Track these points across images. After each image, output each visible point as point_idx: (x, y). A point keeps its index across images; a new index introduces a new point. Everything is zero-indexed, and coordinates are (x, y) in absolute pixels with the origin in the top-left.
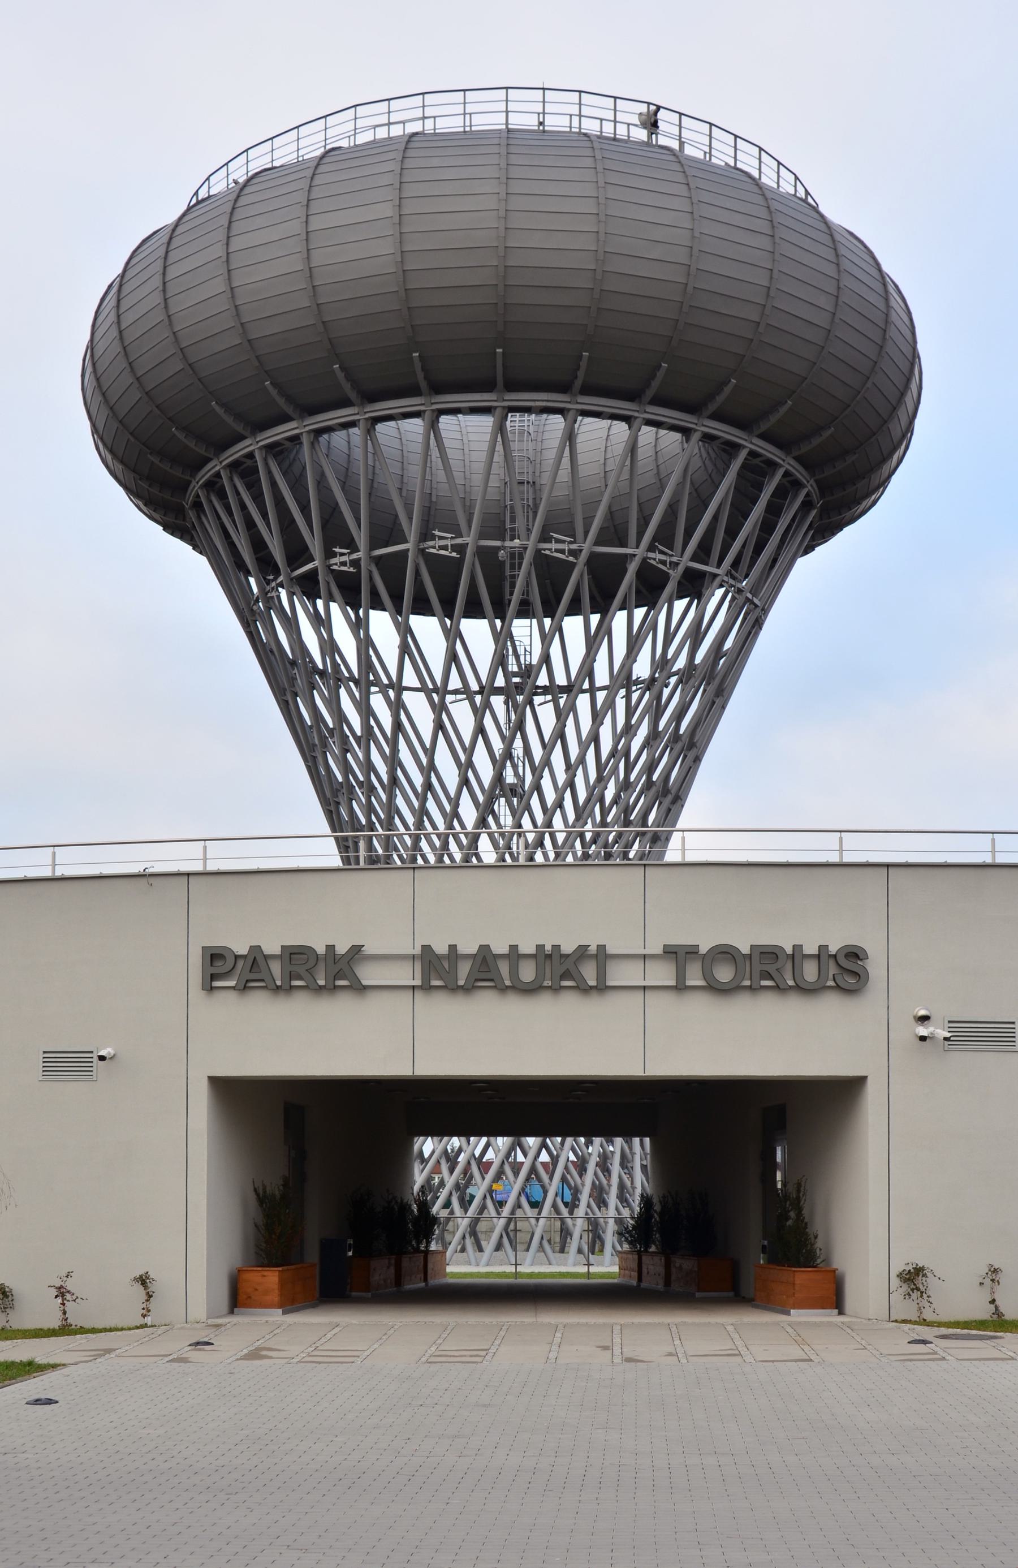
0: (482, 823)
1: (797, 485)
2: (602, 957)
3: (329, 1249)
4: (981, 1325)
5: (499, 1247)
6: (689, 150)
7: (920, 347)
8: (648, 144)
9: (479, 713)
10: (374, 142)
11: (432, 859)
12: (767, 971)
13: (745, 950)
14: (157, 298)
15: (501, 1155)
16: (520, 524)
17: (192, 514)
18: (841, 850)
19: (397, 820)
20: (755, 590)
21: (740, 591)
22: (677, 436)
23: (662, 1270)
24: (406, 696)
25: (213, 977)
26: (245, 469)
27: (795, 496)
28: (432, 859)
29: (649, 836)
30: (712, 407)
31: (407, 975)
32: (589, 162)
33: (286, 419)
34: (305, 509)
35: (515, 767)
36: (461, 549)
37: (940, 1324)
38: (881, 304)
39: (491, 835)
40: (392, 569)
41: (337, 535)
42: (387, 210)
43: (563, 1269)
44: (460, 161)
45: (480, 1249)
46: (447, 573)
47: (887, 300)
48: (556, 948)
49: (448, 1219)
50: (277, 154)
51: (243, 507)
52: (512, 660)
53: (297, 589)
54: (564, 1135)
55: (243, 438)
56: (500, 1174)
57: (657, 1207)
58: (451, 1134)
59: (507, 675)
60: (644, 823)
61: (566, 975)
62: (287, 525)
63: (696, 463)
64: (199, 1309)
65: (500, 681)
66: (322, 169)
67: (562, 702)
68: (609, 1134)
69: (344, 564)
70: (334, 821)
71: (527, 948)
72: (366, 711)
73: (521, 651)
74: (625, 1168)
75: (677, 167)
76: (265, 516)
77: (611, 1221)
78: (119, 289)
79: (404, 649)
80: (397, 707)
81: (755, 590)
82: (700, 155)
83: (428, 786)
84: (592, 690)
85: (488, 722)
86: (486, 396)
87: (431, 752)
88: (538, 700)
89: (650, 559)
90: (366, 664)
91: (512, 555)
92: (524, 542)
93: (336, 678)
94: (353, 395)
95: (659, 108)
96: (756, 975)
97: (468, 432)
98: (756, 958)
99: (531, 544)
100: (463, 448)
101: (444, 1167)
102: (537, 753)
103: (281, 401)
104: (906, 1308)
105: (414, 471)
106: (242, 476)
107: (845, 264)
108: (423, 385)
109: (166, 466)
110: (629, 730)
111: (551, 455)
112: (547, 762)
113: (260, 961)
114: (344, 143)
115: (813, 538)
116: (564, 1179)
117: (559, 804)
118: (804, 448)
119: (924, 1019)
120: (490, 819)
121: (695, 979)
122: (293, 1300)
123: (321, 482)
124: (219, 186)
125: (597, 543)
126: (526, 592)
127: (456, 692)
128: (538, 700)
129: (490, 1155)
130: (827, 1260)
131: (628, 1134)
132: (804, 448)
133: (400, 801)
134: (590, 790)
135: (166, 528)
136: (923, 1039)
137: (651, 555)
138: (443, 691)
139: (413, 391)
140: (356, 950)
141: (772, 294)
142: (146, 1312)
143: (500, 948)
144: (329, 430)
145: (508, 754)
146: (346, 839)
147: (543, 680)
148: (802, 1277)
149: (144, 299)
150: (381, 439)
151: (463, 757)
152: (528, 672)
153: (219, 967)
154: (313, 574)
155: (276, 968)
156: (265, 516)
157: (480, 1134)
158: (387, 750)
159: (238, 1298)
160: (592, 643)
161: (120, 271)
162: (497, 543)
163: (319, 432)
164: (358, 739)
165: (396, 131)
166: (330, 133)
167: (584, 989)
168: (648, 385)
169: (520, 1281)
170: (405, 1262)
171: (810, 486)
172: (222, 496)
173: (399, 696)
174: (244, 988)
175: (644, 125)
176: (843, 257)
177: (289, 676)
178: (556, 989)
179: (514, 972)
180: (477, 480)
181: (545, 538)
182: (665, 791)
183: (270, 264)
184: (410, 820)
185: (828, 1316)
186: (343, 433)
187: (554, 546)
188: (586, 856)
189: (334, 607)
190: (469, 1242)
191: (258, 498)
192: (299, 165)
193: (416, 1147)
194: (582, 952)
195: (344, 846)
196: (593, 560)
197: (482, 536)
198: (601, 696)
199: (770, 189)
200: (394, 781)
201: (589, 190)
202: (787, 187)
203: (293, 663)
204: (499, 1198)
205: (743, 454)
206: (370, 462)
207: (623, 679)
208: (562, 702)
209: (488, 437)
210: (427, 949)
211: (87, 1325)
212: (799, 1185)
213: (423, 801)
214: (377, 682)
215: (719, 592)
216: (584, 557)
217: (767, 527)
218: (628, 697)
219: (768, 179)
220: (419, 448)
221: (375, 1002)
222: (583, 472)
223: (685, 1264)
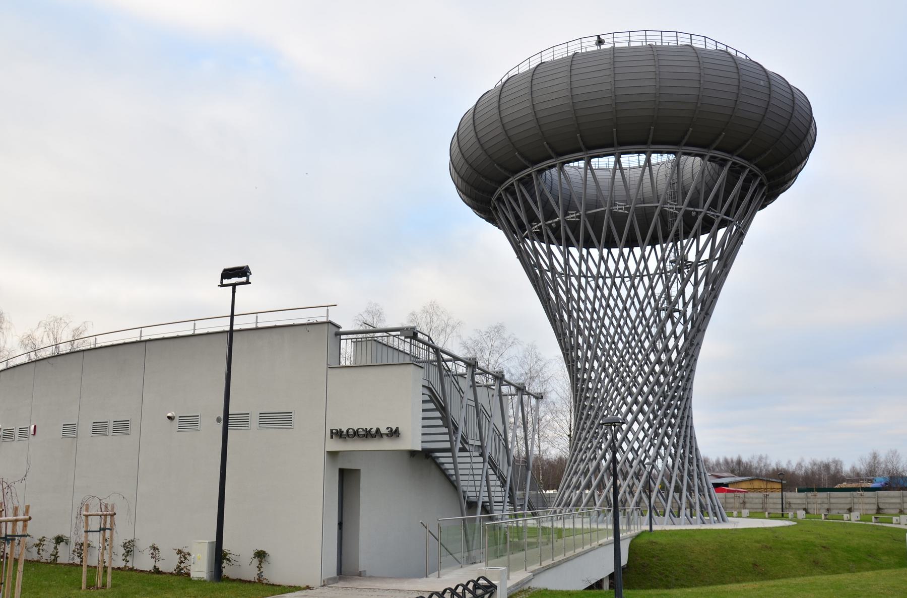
26: (510, 190)
30: (684, 142)
44: (597, 63)
62: (528, 210)
94: (553, 154)
97: (603, 163)
108: (583, 147)
115: (766, 200)
123: (542, 193)
171: (762, 177)
191: (516, 200)
205: (729, 164)
216: (682, 212)
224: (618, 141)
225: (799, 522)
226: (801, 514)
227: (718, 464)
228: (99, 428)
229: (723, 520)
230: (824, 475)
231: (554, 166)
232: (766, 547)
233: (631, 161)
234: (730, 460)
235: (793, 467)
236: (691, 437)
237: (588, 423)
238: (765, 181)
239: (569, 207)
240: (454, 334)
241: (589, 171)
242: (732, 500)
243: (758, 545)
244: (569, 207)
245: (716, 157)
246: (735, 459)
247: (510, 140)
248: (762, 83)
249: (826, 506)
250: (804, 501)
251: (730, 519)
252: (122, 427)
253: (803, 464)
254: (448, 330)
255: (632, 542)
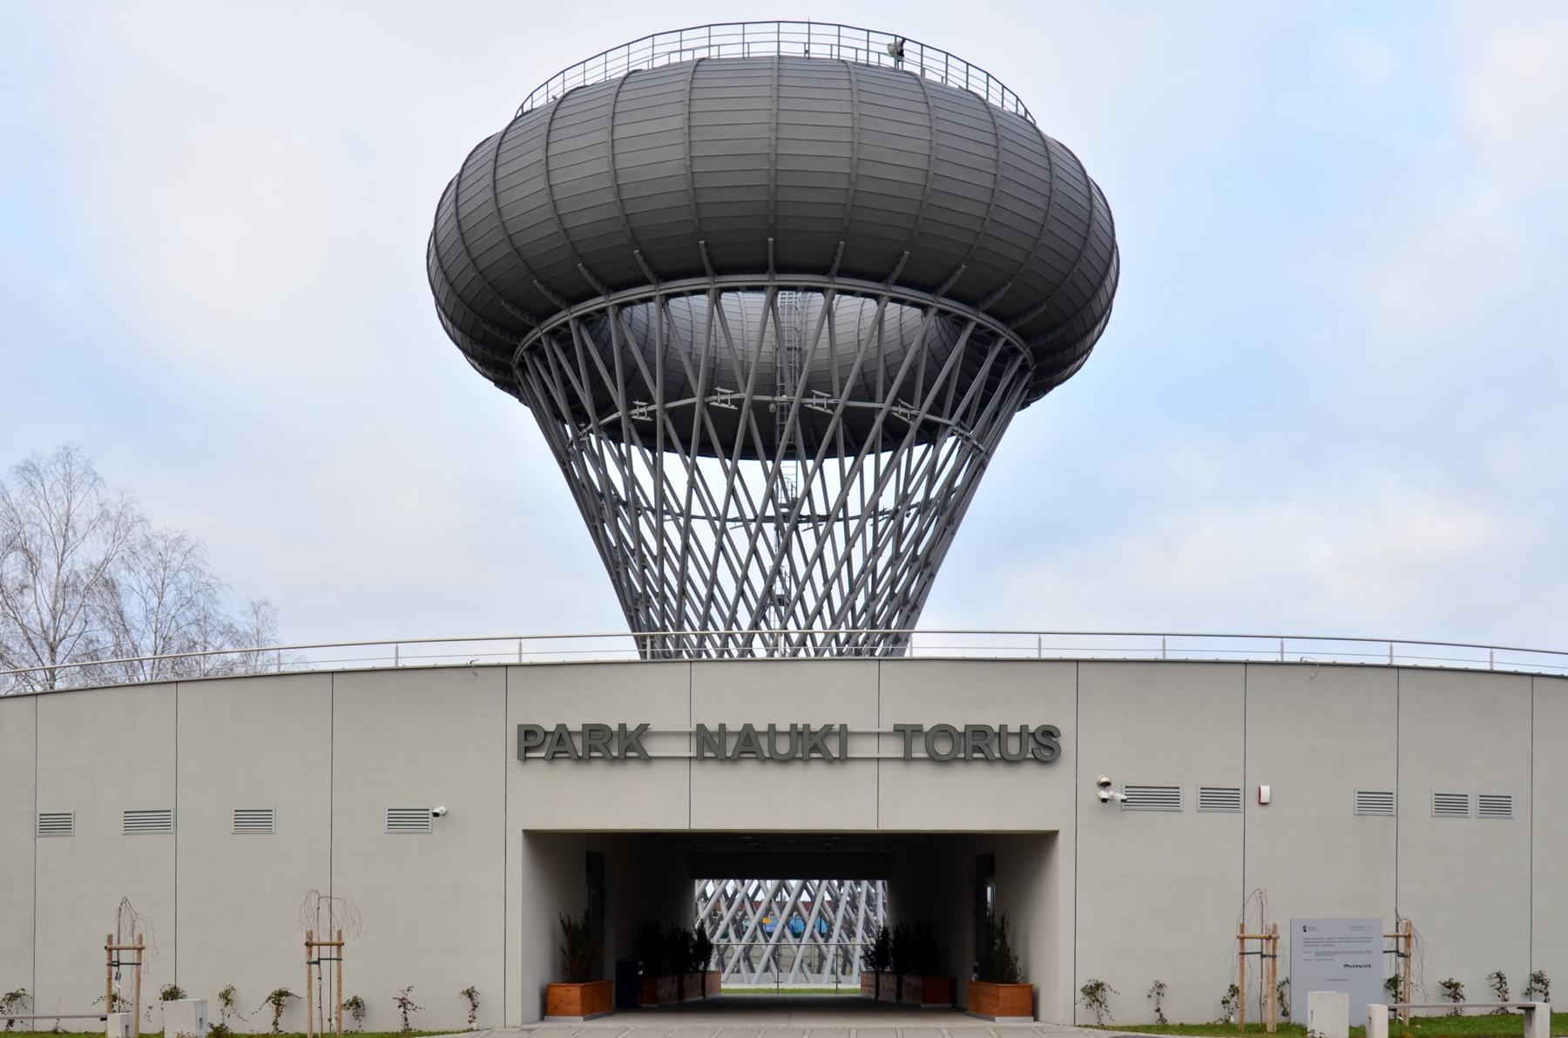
0: (755, 625)
1: (1015, 352)
2: (844, 734)
3: (625, 969)
4: (1148, 1028)
5: (767, 969)
6: (929, 76)
7: (1118, 239)
8: (895, 70)
9: (753, 539)
10: (669, 65)
11: (714, 655)
12: (977, 746)
13: (961, 729)
14: (489, 194)
15: (770, 894)
16: (788, 385)
17: (518, 373)
18: (1040, 649)
19: (686, 625)
20: (980, 439)
21: (967, 439)
22: (918, 311)
23: (894, 986)
24: (694, 523)
25: (527, 749)
26: (561, 336)
27: (1014, 361)
28: (714, 655)
29: (891, 638)
30: (946, 288)
31: (685, 748)
32: (846, 84)
33: (595, 294)
34: (611, 369)
35: (783, 581)
36: (739, 403)
37: (1115, 1028)
38: (1086, 204)
39: (762, 636)
40: (682, 419)
41: (637, 390)
42: (679, 123)
43: (818, 986)
44: (898, 104)
45: (753, 971)
46: (726, 421)
47: (1091, 200)
48: (807, 726)
49: (727, 946)
50: (588, 75)
51: (560, 367)
52: (781, 494)
53: (604, 435)
54: (821, 878)
56: (768, 910)
57: (892, 936)
58: (729, 877)
59: (776, 507)
60: (888, 626)
61: (815, 749)
63: (933, 334)
64: (515, 1017)
65: (770, 512)
66: (625, 87)
67: (821, 529)
68: (857, 877)
69: (642, 414)
70: (634, 623)
71: (783, 726)
72: (660, 534)
73: (789, 487)
74: (869, 904)
75: (919, 89)
76: (578, 375)
77: (858, 948)
78: (457, 186)
79: (692, 485)
80: (686, 532)
81: (980, 439)
82: (938, 79)
83: (711, 597)
84: (846, 519)
85: (761, 543)
87: (714, 568)
88: (802, 526)
90: (661, 497)
91: (782, 408)
92: (790, 397)
93: (635, 508)
94: (650, 275)
95: (904, 40)
96: (969, 749)
97: (744, 307)
98: (969, 736)
99: (796, 399)
100: (740, 319)
101: (723, 905)
102: (801, 570)
103: (591, 280)
104: (1088, 1016)
105: (701, 338)
106: (559, 342)
107: (1057, 171)
108: (708, 267)
109: (496, 333)
110: (877, 552)
111: (813, 326)
112: (809, 576)
113: (565, 736)
114: (644, 67)
116: (820, 914)
117: (819, 611)
118: (1022, 322)
119: (1105, 785)
120: (763, 624)
121: (919, 751)
122: (591, 1010)
123: (624, 347)
124: (540, 101)
125: (850, 399)
126: (792, 437)
127: (735, 520)
128: (802, 526)
129: (760, 897)
130: (1026, 978)
131: (872, 878)
132: (1022, 322)
133: (688, 609)
134: (845, 601)
135: (497, 384)
136: (1104, 800)
138: (724, 519)
139: (699, 272)
140: (643, 728)
142: (472, 1019)
143: (761, 726)
144: (631, 304)
145: (777, 570)
146: (644, 638)
147: (805, 511)
148: (1005, 991)
149: (479, 195)
150: (673, 312)
151: (739, 572)
152: (794, 504)
153: (531, 740)
154: (617, 422)
155: (578, 743)
156: (578, 375)
157: (752, 877)
158: (677, 566)
159: (548, 1008)
160: (846, 483)
161: (458, 171)
162: (768, 398)
163: (622, 306)
164: (654, 558)
165: (687, 57)
166: (632, 58)
167: (829, 760)
168: (893, 269)
169: (781, 995)
170: (687, 980)
171: (1026, 353)
172: (543, 358)
173: (688, 522)
174: (552, 758)
175: (892, 54)
176: (1054, 164)
177: (597, 506)
178: (806, 760)
179: (772, 746)
180: (753, 346)
181: (807, 394)
182: (905, 601)
183: (582, 168)
184: (697, 624)
185: (1026, 1022)
186: (643, 306)
187: (815, 401)
188: (840, 653)
189: (634, 449)
190: (743, 966)
191: (572, 360)
192: (607, 84)
193: (698, 891)
194: (827, 730)
195: (641, 642)
196: (847, 412)
197: (756, 392)
198: (853, 524)
199: (995, 108)
200: (683, 591)
201: (847, 108)
202: (1010, 106)
203: (601, 496)
204: (768, 929)
205: (971, 326)
206: (665, 330)
207: (872, 510)
208: (821, 529)
209: (761, 311)
210: (701, 727)
211: (424, 1030)
212: (1003, 918)
213: (707, 609)
214: (670, 511)
215: (951, 440)
216: (839, 410)
217: (990, 387)
218: (875, 525)
219: (994, 100)
220: (704, 319)
221: (657, 768)
222: (839, 340)
223: (913, 981)
228: (1450, 804)
231: (650, 299)
247: (568, 236)
252: (1497, 806)
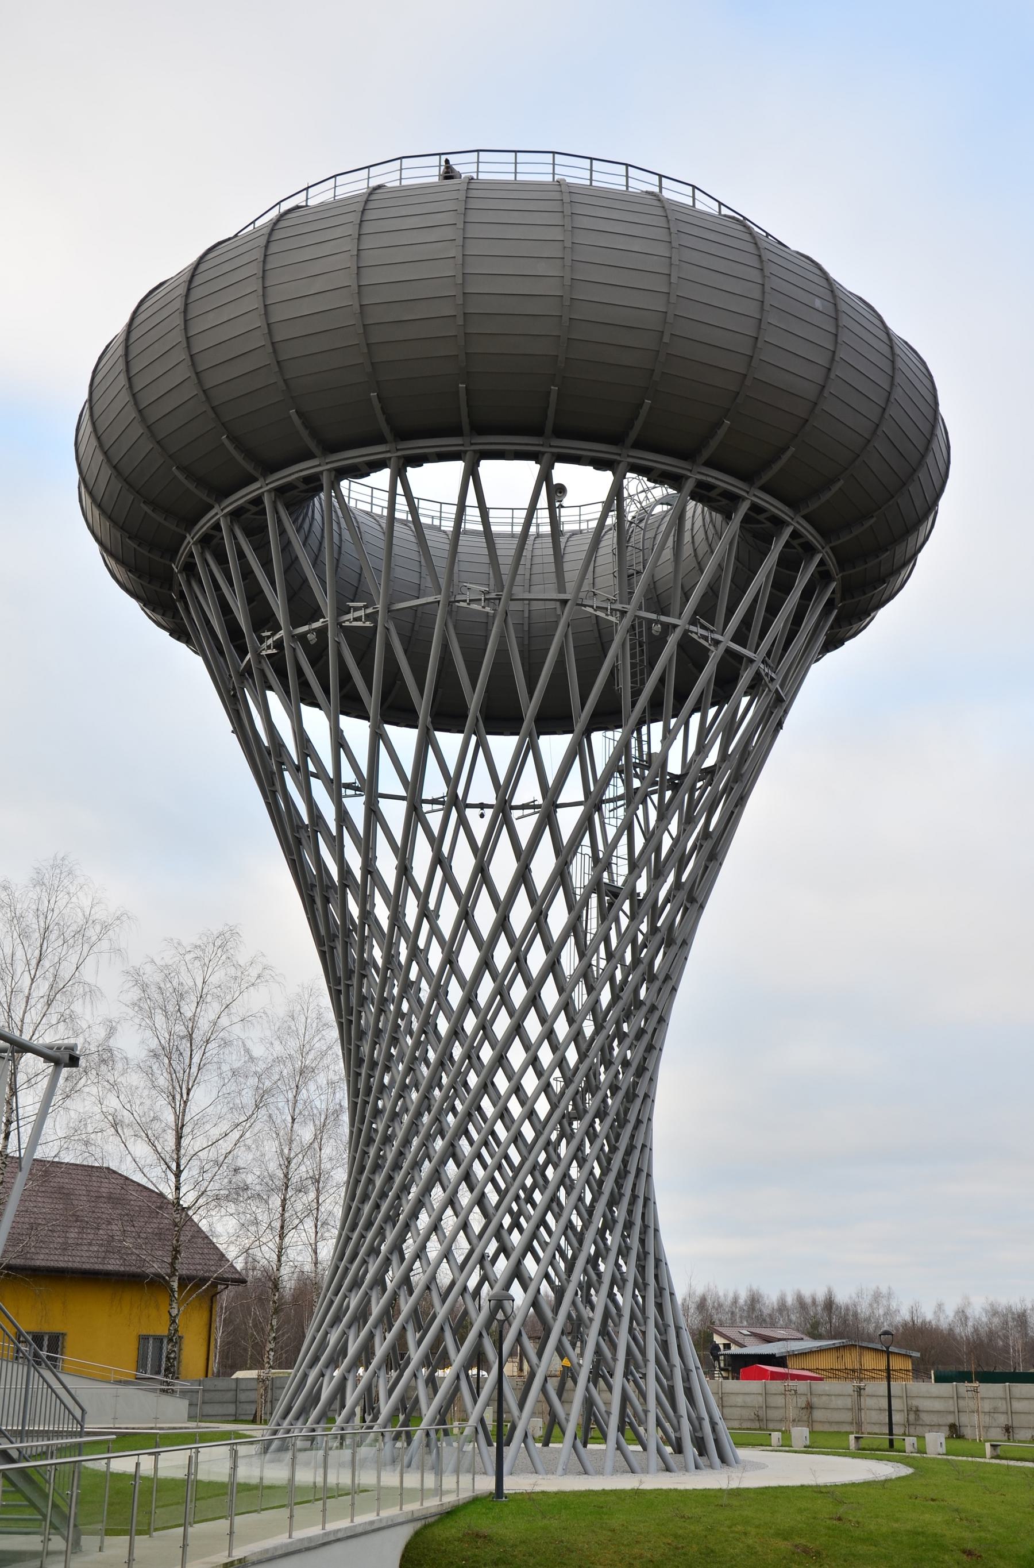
55: (255, 480)
62: (254, 596)
86: (786, 509)
89: (692, 632)
97: (436, 482)
118: (813, 505)
137: (693, 628)
139: (379, 439)
141: (759, 345)
172: (222, 559)
183: (231, 320)
191: (267, 564)
202: (712, 208)
205: (744, 508)
216: (627, 621)
224: (474, 431)
225: (921, 1467)
226: (936, 1442)
227: (782, 1307)
229: (723, 1459)
230: (1016, 1342)
232: (806, 1551)
233: (508, 481)
234: (808, 1300)
235: (946, 1319)
236: (645, 1228)
237: (379, 1181)
238: (832, 565)
239: (352, 591)
240: (104, 944)
241: (401, 501)
242: (779, 1401)
243: (784, 1546)
244: (352, 591)
245: (710, 487)
246: (821, 1297)
247: (208, 399)
248: (818, 304)
249: (1002, 1420)
250: (951, 1405)
251: (743, 1453)
253: (969, 1312)
254: (92, 933)
255: (417, 1534)
